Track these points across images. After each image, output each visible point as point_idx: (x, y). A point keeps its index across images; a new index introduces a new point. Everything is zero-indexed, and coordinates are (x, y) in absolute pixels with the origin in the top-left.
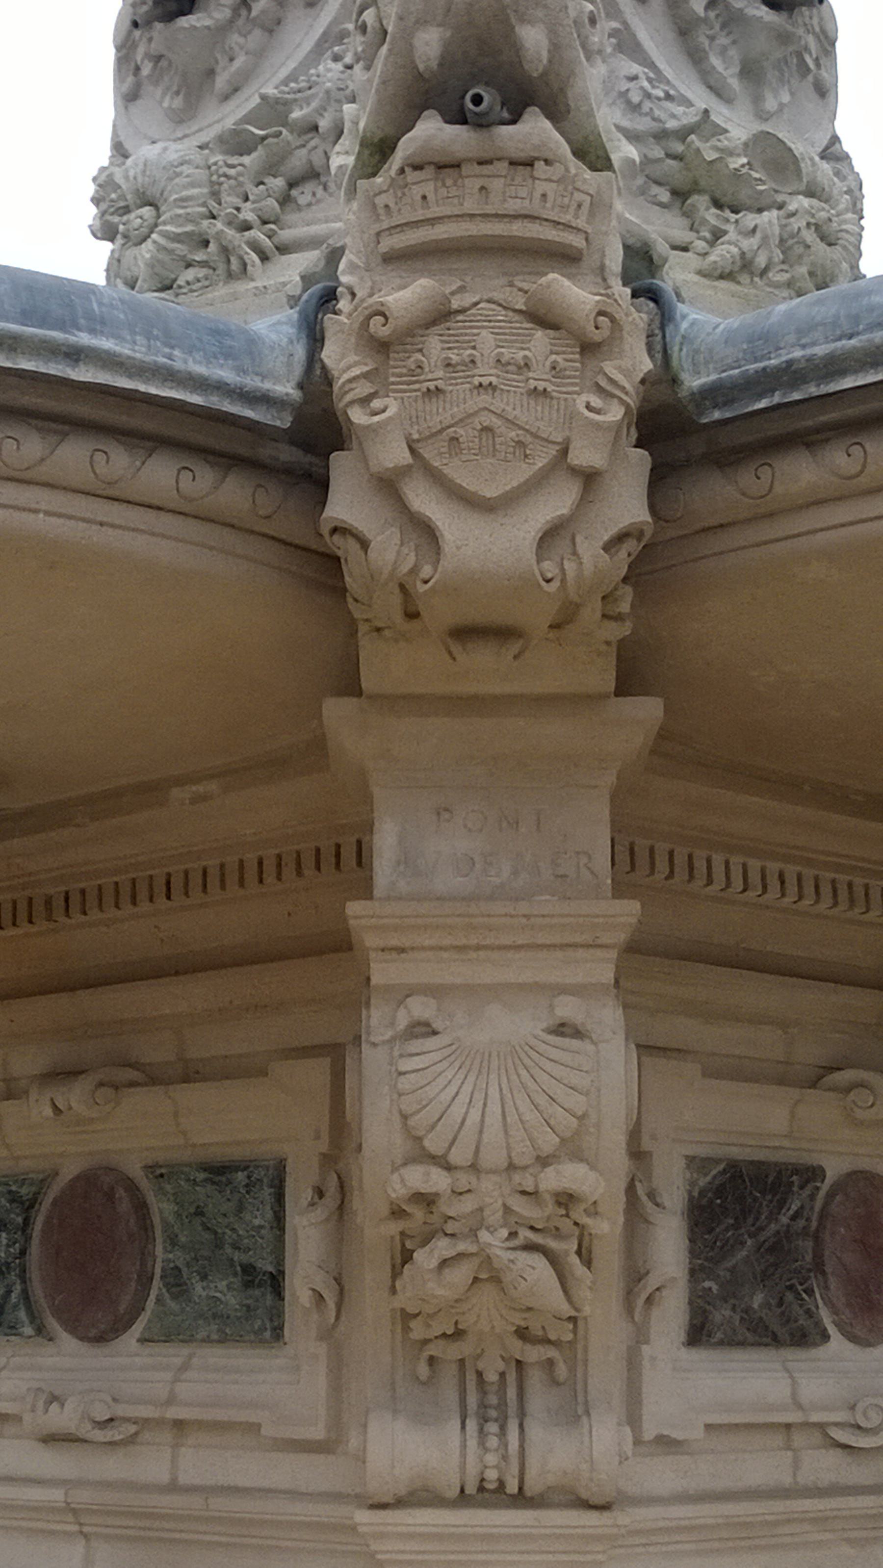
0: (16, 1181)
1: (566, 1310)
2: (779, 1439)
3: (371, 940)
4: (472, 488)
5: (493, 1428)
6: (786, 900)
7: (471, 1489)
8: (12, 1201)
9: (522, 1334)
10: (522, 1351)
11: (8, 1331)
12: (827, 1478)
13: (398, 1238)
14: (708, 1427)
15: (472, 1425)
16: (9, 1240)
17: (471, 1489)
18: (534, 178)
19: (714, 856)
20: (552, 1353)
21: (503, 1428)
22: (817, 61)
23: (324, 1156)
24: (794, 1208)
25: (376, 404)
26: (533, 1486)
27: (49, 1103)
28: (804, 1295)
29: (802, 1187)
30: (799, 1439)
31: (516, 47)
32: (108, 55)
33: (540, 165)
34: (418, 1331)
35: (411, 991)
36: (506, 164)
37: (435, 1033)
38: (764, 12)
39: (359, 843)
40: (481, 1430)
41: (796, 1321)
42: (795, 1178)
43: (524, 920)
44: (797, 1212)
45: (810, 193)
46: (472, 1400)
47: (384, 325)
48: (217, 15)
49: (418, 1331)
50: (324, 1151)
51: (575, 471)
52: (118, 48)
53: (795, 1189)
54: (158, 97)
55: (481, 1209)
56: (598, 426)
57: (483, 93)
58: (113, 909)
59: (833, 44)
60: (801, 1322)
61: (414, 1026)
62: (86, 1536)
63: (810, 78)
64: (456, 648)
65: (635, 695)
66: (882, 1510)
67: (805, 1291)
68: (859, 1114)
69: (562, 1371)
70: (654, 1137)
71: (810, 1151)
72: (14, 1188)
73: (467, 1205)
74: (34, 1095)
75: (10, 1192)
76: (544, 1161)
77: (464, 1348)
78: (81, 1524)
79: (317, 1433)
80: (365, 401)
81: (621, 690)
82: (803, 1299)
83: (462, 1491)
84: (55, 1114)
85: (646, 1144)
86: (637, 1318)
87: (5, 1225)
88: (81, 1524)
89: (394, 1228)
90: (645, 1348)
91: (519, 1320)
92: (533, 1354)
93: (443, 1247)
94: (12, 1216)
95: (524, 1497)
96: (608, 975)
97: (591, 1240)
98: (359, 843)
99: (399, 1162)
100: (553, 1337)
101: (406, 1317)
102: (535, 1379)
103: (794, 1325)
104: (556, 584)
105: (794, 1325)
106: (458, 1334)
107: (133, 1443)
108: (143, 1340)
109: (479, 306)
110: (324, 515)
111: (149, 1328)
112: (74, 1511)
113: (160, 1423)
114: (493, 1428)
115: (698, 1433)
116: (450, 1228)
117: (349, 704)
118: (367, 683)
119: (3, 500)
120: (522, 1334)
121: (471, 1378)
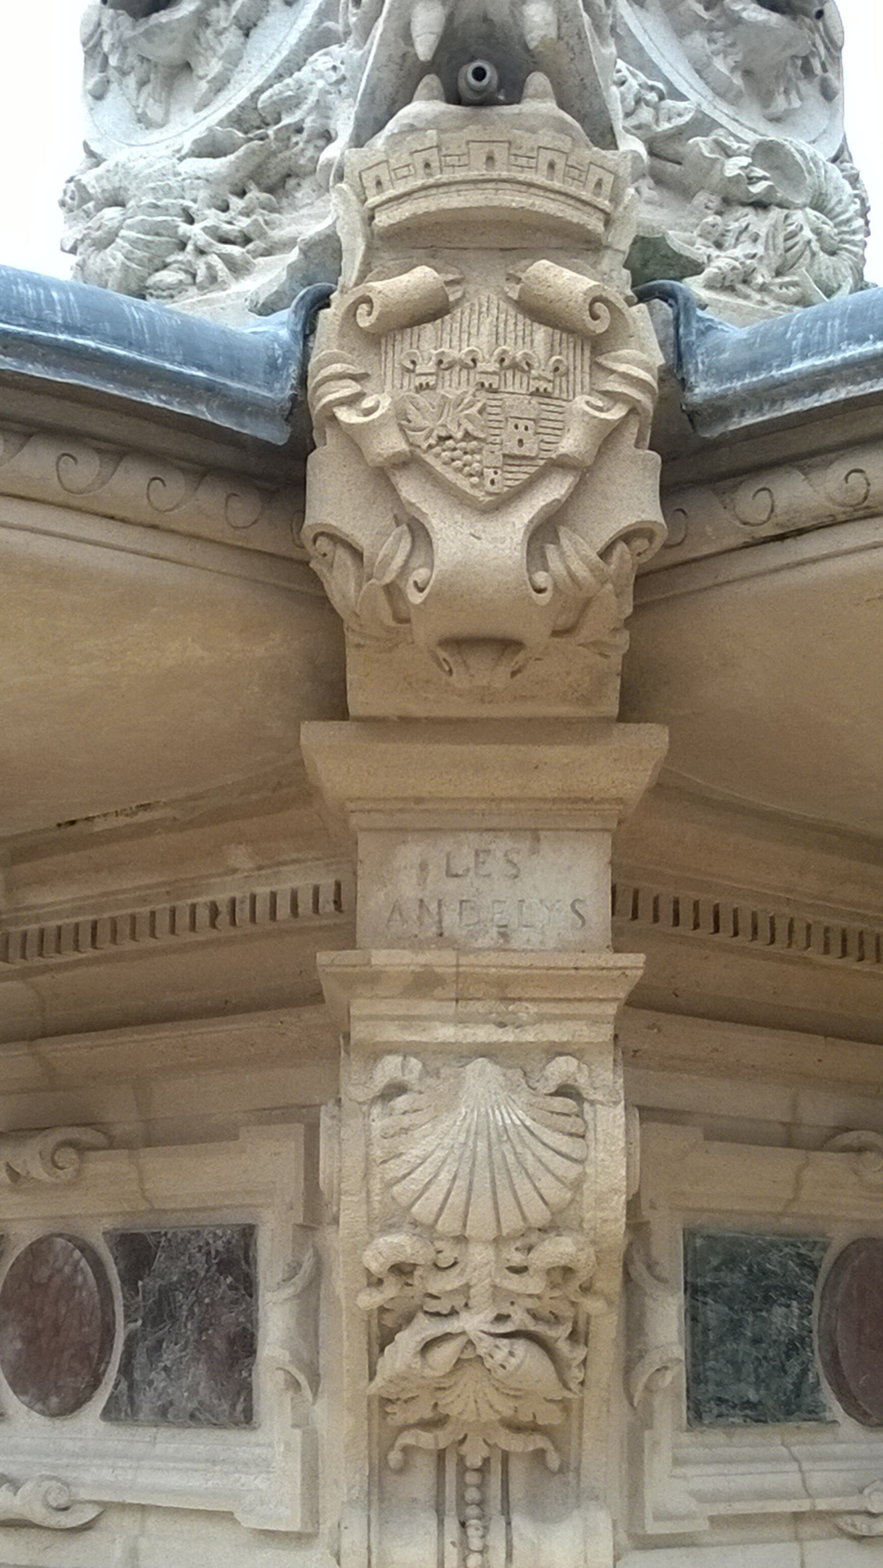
0: (804, 1244)
1: (559, 1393)
2: (785, 1531)
8: (802, 1265)
11: (805, 1415)
13: (376, 1314)
14: (713, 1520)
16: (801, 1310)
20: (539, 1442)
22: (823, 65)
23: (302, 1226)
25: (367, 403)
35: (391, 1049)
43: (573, 972)
46: (450, 1491)
50: (300, 1220)
55: (468, 1286)
57: (488, 74)
59: (839, 49)
63: (817, 80)
69: (553, 1460)
70: (653, 1207)
72: (802, 1251)
73: (448, 1282)
75: (799, 1255)
80: (351, 401)
84: (11, 1179)
85: (646, 1213)
87: (796, 1293)
90: (647, 1434)
94: (803, 1282)
96: (606, 1032)
102: (518, 1472)
106: (437, 1422)
111: (192, 1416)
115: (705, 1526)
116: (432, 1306)
118: (352, 711)
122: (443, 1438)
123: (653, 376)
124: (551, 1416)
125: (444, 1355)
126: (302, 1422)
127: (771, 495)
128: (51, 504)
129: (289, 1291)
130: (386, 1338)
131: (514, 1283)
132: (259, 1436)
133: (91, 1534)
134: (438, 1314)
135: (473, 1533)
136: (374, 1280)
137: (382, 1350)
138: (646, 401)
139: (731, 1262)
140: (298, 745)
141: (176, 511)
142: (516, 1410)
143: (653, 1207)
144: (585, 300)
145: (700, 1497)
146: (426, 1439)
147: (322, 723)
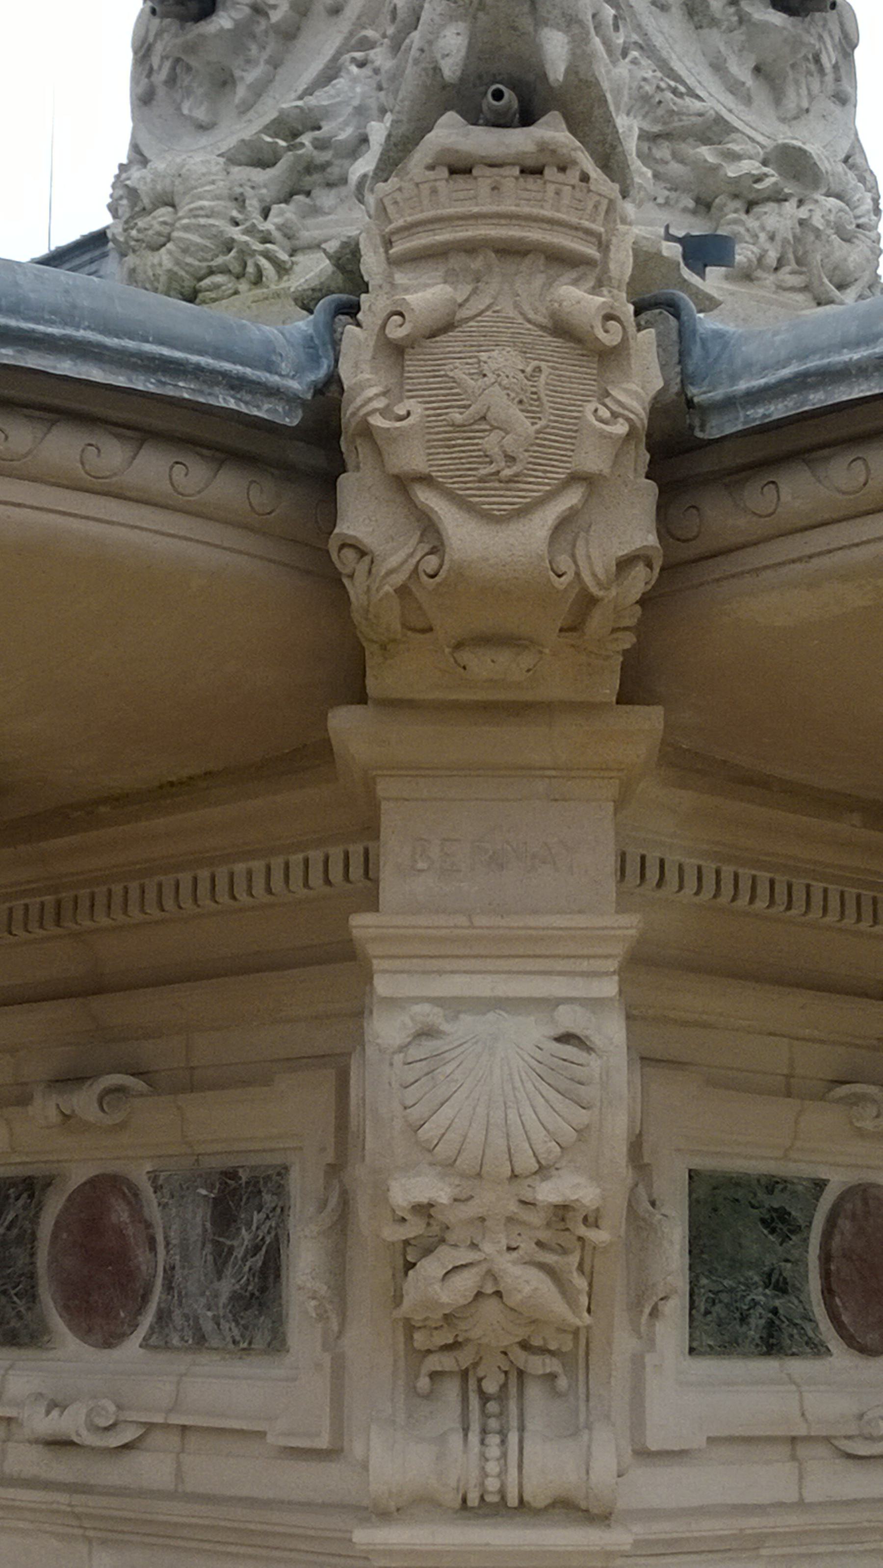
3: (372, 949)
6: (793, 912)
10: (526, 1361)
12: (30, 1471)
15: (474, 1437)
17: (473, 1499)
19: (724, 868)
24: (10, 1217)
27: (54, 1106)
28: (15, 1299)
29: (17, 1199)
30: (802, 1451)
31: (537, 49)
32: (125, 58)
33: (550, 173)
34: (420, 1340)
38: (777, 18)
39: (366, 852)
41: (8, 1323)
42: (12, 1190)
44: (12, 1222)
48: (237, 15)
49: (420, 1340)
52: (135, 53)
53: (11, 1201)
56: (609, 436)
59: (854, 46)
60: (12, 1324)
62: (89, 1541)
65: (648, 705)
66: (880, 1524)
67: (16, 1294)
69: (562, 1383)
71: (59, 1161)
74: (38, 1101)
76: (543, 1171)
77: (465, 1358)
79: (323, 1442)
81: (623, 698)
82: (14, 1303)
83: (464, 1500)
86: (643, 1329)
92: (537, 1365)
93: (447, 1257)
98: (366, 852)
100: (553, 1347)
101: (410, 1328)
103: (7, 1327)
105: (7, 1327)
109: (484, 314)
113: (166, 1426)
117: (357, 711)
146: (447, 1362)
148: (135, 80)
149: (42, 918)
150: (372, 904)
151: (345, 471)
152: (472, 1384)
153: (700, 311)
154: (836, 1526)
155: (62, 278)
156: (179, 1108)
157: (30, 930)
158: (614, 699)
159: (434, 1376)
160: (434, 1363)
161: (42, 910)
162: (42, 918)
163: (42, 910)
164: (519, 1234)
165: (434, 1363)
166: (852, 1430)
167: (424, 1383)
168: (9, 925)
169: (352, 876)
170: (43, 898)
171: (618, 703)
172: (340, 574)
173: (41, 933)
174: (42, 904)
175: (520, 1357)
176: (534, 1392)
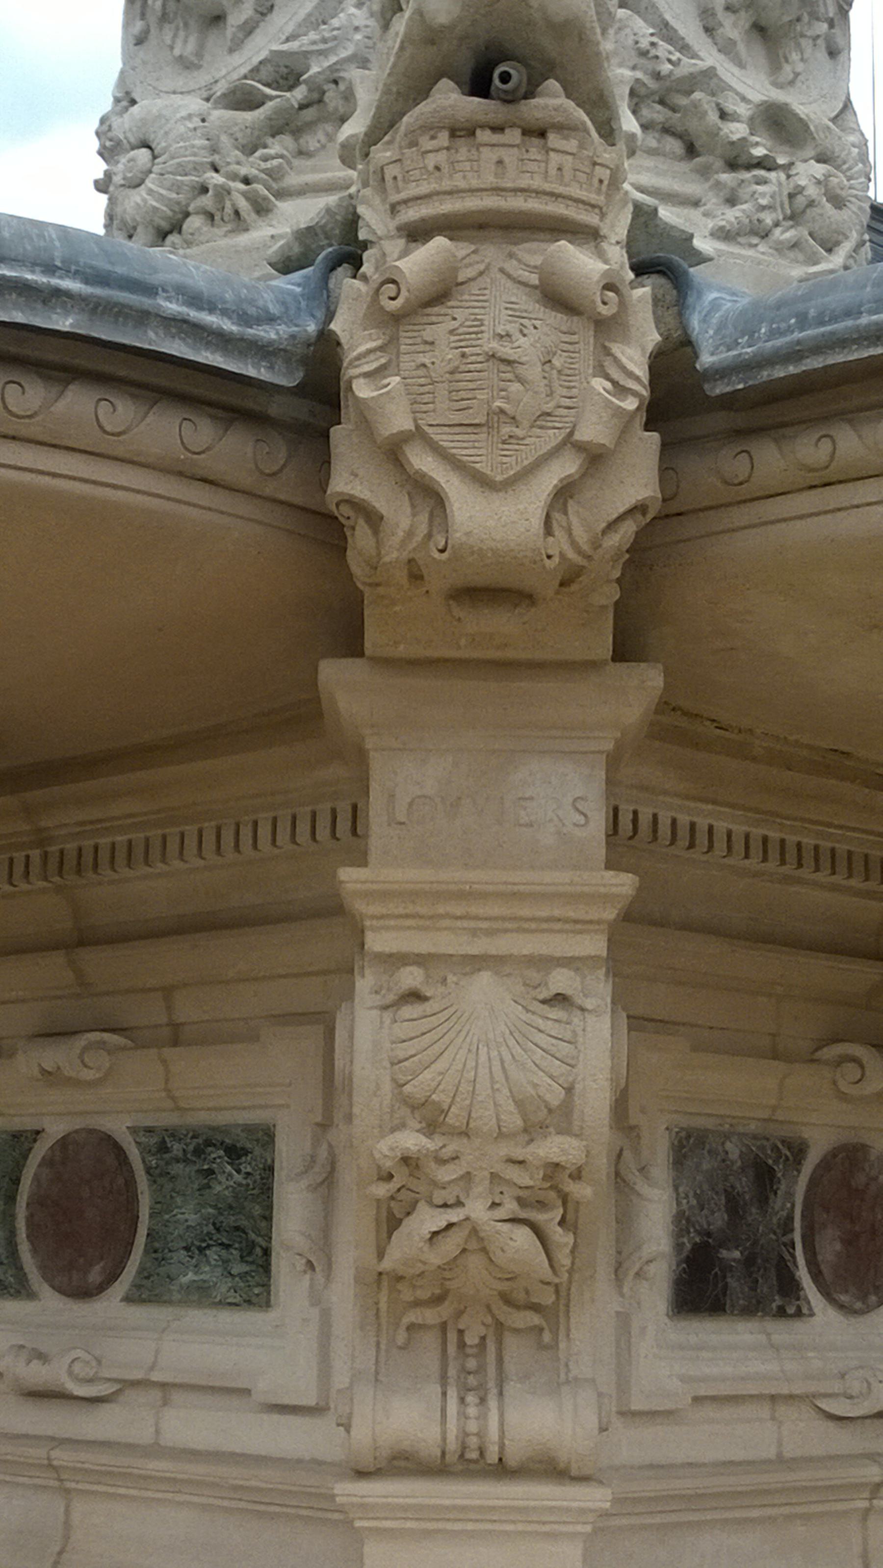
4: (467, 656)
5: (473, 1441)
7: (451, 1458)
9: (507, 1299)
17: (451, 1458)
18: (548, 150)
21: (483, 1400)
26: (512, 1461)
36: (517, 132)
37: (425, 999)
39: (355, 808)
40: (462, 1400)
45: (821, 159)
47: (393, 299)
51: (580, 447)
54: (168, 40)
57: (507, 69)
58: (109, 872)
61: (394, 1458)
64: (457, 612)
68: (843, 1086)
69: (547, 1337)
78: (62, 1480)
88: (62, 1480)
89: (382, 1190)
91: (505, 1286)
95: (504, 1467)
97: (577, 1211)
98: (355, 808)
99: (405, 477)
104: (556, 559)
107: (44, 302)
108: (128, 1299)
110: (329, 492)
112: (56, 1469)
114: (473, 1441)
119: (3, 430)
120: (507, 1299)
121: (452, 1337)
122: (445, 1311)
123: (645, 387)
124: (547, 1298)
125: (451, 1245)
126: (316, 1299)
127: (834, 443)
128: (116, 459)
129: (304, 1183)
130: (393, 1223)
131: (513, 1174)
132: (272, 1315)
133: (106, 1406)
134: (445, 1205)
135: (472, 1411)
136: (385, 1174)
137: (390, 1237)
138: (645, 393)
139: (309, 345)
140: (315, 684)
141: (203, 456)
142: (512, 1231)
143: (643, 1111)
144: (598, 282)
145: (683, 1379)
146: (430, 1316)
147: (350, 660)
148: (127, 24)
149: (113, 857)
150: (361, 860)
151: (339, 423)
152: (452, 1337)
153: (691, 266)
154: (122, 1491)
155: (425, 110)
156: (164, 1062)
157: (15, 883)
158: (609, 657)
159: (411, 1327)
160: (412, 1317)
161: (80, 856)
162: (113, 857)
163: (80, 856)
164: (502, 1193)
165: (412, 1317)
166: (836, 1387)
167: (401, 1337)
168: (11, 875)
169: (299, 840)
170: (148, 834)
171: (614, 659)
172: (343, 526)
173: (24, 886)
174: (113, 845)
175: (504, 1313)
176: (513, 1344)
